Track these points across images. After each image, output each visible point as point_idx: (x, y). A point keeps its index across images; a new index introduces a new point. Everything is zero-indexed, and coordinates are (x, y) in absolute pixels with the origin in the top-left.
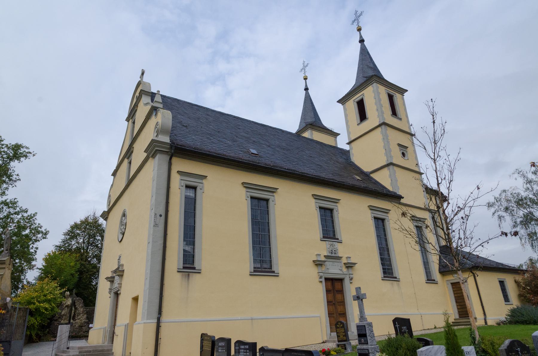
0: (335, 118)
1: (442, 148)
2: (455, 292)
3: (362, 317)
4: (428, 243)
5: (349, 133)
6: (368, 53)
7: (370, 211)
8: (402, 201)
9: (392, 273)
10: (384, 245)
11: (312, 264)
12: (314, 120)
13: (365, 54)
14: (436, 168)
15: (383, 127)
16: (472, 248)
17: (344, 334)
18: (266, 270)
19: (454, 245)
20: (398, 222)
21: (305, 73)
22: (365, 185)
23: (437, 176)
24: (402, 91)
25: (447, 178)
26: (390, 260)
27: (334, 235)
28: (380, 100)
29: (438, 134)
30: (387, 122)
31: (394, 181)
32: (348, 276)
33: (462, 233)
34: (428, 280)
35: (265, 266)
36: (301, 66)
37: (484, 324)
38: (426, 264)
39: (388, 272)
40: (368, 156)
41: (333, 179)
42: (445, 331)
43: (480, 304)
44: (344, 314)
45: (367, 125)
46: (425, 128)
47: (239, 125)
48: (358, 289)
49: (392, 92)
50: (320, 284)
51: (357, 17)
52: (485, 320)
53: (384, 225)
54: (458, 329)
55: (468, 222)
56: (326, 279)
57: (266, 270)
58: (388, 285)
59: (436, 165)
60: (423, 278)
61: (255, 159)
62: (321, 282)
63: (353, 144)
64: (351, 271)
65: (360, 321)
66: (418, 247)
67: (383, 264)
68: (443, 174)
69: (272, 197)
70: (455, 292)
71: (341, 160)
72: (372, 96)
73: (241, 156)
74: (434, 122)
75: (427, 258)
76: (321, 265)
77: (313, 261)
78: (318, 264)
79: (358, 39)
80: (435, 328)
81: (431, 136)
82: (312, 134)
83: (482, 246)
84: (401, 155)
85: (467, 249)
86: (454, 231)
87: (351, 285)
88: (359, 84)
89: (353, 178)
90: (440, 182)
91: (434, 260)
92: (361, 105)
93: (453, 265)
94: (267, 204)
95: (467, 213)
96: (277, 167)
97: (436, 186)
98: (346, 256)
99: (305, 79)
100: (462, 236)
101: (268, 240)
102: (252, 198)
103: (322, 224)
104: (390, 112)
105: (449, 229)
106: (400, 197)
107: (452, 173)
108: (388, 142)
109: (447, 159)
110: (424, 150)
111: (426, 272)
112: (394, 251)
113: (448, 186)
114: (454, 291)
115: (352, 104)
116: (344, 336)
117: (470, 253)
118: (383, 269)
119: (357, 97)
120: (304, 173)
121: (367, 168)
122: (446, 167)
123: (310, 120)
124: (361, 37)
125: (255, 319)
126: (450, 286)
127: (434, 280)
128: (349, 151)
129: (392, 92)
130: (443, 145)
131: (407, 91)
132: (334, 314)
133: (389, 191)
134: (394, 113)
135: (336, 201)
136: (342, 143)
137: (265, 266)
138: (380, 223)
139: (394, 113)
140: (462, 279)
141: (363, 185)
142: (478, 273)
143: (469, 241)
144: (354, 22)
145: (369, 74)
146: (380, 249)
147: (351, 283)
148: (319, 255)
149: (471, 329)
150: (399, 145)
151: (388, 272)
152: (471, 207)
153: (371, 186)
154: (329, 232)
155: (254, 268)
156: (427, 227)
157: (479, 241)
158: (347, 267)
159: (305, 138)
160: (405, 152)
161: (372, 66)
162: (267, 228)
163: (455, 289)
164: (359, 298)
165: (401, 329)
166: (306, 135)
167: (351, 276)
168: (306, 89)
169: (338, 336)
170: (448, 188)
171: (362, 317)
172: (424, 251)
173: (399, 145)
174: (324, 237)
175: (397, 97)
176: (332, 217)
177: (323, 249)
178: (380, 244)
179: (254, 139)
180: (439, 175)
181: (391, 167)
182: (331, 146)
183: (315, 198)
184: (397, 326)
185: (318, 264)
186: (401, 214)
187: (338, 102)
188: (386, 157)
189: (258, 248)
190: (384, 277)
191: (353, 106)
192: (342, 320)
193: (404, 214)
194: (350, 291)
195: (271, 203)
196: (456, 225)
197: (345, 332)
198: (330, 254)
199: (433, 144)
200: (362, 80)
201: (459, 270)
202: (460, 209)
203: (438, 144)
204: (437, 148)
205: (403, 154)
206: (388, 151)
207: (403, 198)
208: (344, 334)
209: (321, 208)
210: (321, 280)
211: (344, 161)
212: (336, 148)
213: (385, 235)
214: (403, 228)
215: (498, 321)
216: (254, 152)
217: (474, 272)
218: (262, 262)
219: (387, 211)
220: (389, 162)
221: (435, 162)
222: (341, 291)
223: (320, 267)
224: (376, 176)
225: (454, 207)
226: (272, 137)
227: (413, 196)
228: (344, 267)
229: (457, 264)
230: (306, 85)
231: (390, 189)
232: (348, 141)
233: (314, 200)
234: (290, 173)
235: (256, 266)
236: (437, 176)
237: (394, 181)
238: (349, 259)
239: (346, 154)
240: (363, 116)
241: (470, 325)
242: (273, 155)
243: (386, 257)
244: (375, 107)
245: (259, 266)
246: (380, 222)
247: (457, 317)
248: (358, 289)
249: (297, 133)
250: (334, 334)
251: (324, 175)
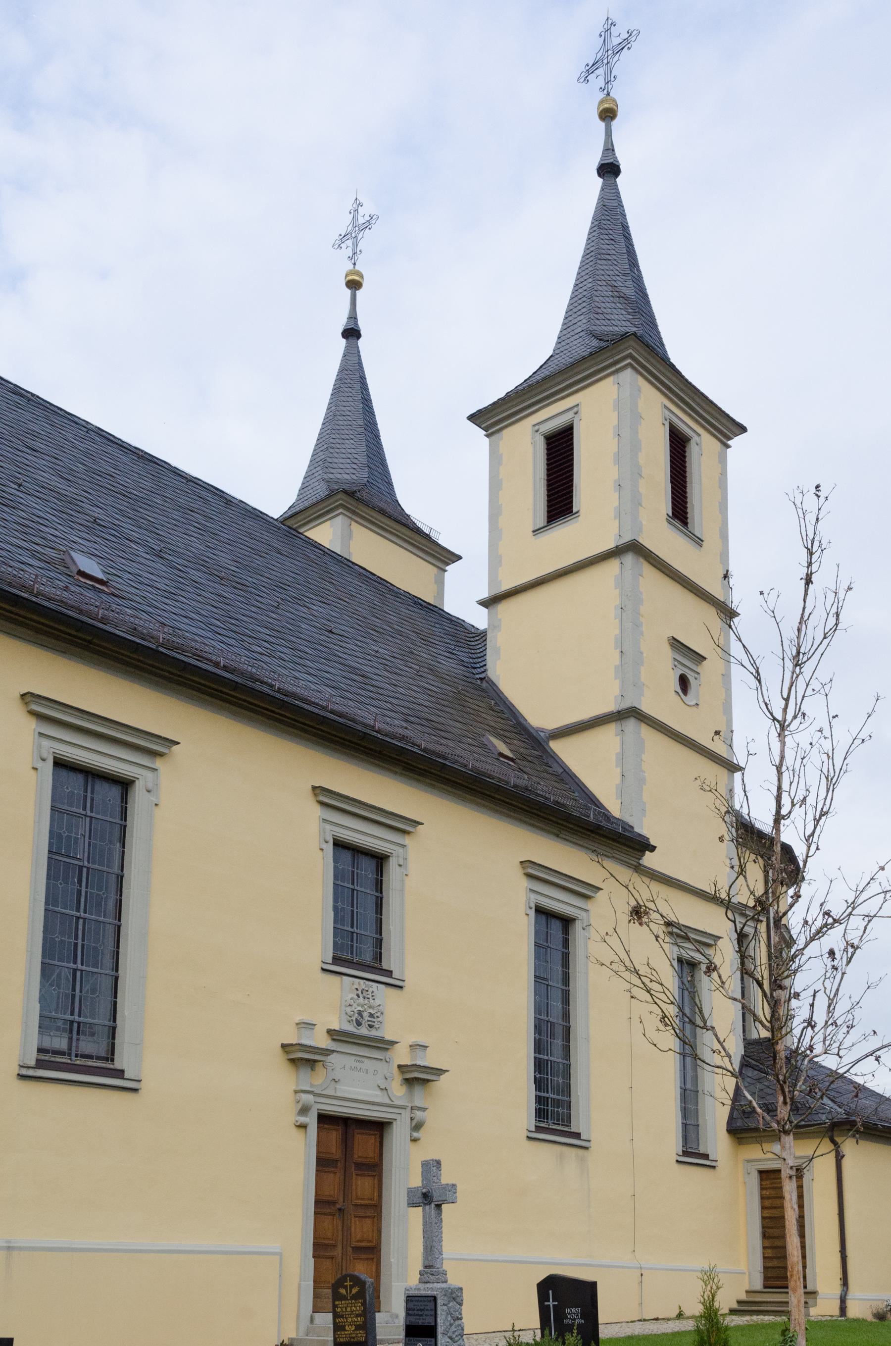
0: (451, 480)
1: (817, 687)
2: (767, 1203)
3: (431, 1268)
4: (705, 1027)
5: (495, 560)
6: (625, 228)
7: (525, 883)
8: (649, 860)
9: (567, 1119)
10: (555, 1017)
11: (279, 1058)
12: (363, 475)
13: (611, 231)
14: (782, 757)
15: (629, 559)
16: (845, 1061)
17: (360, 1320)
18: (90, 1063)
19: (791, 1041)
20: (613, 941)
21: (353, 257)
22: (522, 781)
23: (779, 788)
24: (727, 428)
25: (811, 800)
26: (567, 1072)
27: (378, 957)
28: (636, 447)
29: (817, 624)
30: (646, 541)
31: (631, 779)
32: (406, 1115)
33: (822, 1003)
34: (686, 1153)
35: (87, 1045)
36: (343, 224)
37: (837, 1312)
38: (690, 1098)
39: (553, 1111)
40: (552, 669)
41: (403, 738)
42: (698, 1331)
43: (838, 1248)
44: (372, 1251)
46: (774, 594)
47: (35, 435)
48: (432, 1167)
49: (687, 424)
50: (299, 1135)
51: (603, 62)
52: (843, 1301)
53: (566, 943)
54: (738, 1328)
55: (849, 969)
56: (324, 1119)
57: (90, 1063)
58: (546, 1156)
59: (783, 744)
60: (673, 1143)
61: (91, 602)
62: (303, 1127)
63: (503, 607)
64: (419, 1097)
65: (421, 1281)
66: (669, 1040)
67: (539, 1084)
68: (802, 786)
69: (149, 775)
70: (767, 1203)
71: (448, 665)
72: (612, 420)
73: (28, 575)
74: (808, 581)
75: (695, 1079)
76: (311, 1064)
77: (284, 1046)
78: (302, 1058)
79: (596, 159)
80: (680, 1316)
81: (790, 632)
82: (347, 537)
83: (877, 1059)
84: (675, 685)
85: (830, 1062)
86: (797, 995)
87: (412, 1146)
88: (566, 360)
89: (484, 746)
90: (784, 812)
91: (719, 1090)
92: (560, 448)
93: (770, 1109)
94: (124, 799)
95: (854, 937)
96: (181, 649)
97: (770, 821)
98: (412, 1040)
99: (354, 285)
100: (820, 1018)
101: (111, 947)
102: (60, 764)
103: (335, 909)
104: (665, 505)
105: (781, 987)
106: (643, 846)
107: (831, 783)
108: (637, 625)
109: (826, 732)
110: (754, 683)
111: (685, 1126)
112: (587, 1040)
113: (809, 831)
114: (763, 1198)
115: (525, 442)
116: (358, 1328)
117: (835, 1076)
118: (539, 1100)
119: (551, 416)
120: (294, 695)
121: (540, 716)
122: (816, 759)
123: (350, 473)
124: (609, 149)
125: (20, 1249)
126: (755, 1179)
127: (706, 1156)
128: (481, 636)
129: (687, 424)
130: (823, 675)
131: (743, 429)
132: (334, 1246)
133: (607, 816)
134: (680, 512)
135: (401, 826)
136: (462, 595)
137: (87, 1045)
138: (555, 930)
139: (680, 512)
140: (791, 1162)
141: (514, 779)
142: (849, 1146)
143: (840, 1036)
144: (591, 69)
145: (613, 327)
146: (538, 1028)
147: (415, 1140)
148: (311, 1026)
149: (785, 1332)
150: (676, 644)
151: (553, 1111)
152: (870, 918)
153: (546, 789)
154: (360, 943)
155: (40, 1050)
156: (711, 968)
157: (872, 1038)
158: (410, 1082)
159: (317, 546)
160: (691, 676)
161: (630, 292)
162: (113, 897)
163: (767, 1193)
164: (430, 1199)
165: (560, 1315)
166: (326, 533)
167: (419, 1115)
168: (352, 333)
169: (337, 1328)
170: (809, 839)
171: (431, 1268)
172: (689, 1054)
173: (676, 644)
174: (336, 960)
175: (703, 446)
176: (379, 885)
177: (329, 1003)
178: (541, 1008)
179: (97, 513)
180: (785, 786)
181: (631, 725)
183: (322, 804)
184: (551, 1303)
185: (302, 1058)
186: (628, 910)
187: (472, 418)
188: (617, 684)
189: (66, 974)
190: (538, 1129)
191: (530, 449)
192: (361, 1270)
193: (638, 913)
194: (403, 1169)
195: (139, 798)
196: (808, 976)
197: (364, 1314)
198: (351, 1028)
199: (789, 665)
200: (581, 347)
201: (787, 1133)
202: (831, 921)
203: (808, 669)
204: (801, 684)
205: (684, 682)
206: (629, 662)
207: (653, 849)
208: (360, 1320)
209: (339, 845)
210: (303, 1120)
211: (460, 670)
212: (433, 611)
213: (566, 980)
214: (628, 963)
215: (882, 1306)
216: (93, 568)
217: (838, 1139)
218: (75, 1029)
219: (585, 891)
220: (626, 705)
221: (781, 736)
222: (374, 1168)
223: (305, 1072)
224: (571, 753)
225: (815, 911)
226: (176, 515)
227: (690, 847)
228: (398, 1078)
229: (783, 1112)
230: (353, 317)
231: (614, 808)
232: (485, 594)
233: (317, 812)
234: (236, 686)
235: (47, 1044)
236: (779, 788)
237: (631, 779)
238: (419, 1052)
239: (469, 642)
240: (559, 502)
241: (787, 1313)
242: (169, 595)
243: (556, 1057)
244: (614, 473)
245: (61, 1043)
246: (556, 926)
247: (758, 1285)
248: (432, 1167)
249: (286, 519)
250: (326, 1319)
251: (369, 715)
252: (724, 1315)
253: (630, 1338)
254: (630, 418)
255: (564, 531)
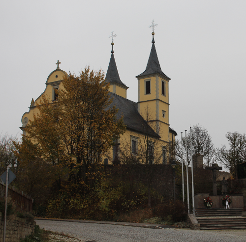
8: (160, 139)
40: (147, 111)
45: (149, 97)
49: (164, 80)
72: (155, 81)
92: (148, 84)
99: (113, 44)
115: (143, 81)
119: (147, 79)
134: (163, 93)
139: (163, 93)
145: (154, 67)
168: (112, 52)
173: (163, 111)
182: (123, 98)
205: (164, 115)
240: (148, 91)
252: (104, 83)
253: (100, 220)
254: (157, 81)
255: (148, 95)
